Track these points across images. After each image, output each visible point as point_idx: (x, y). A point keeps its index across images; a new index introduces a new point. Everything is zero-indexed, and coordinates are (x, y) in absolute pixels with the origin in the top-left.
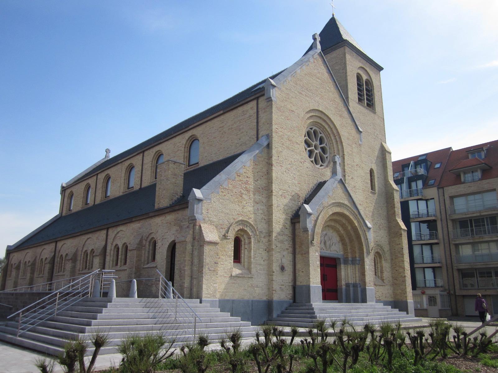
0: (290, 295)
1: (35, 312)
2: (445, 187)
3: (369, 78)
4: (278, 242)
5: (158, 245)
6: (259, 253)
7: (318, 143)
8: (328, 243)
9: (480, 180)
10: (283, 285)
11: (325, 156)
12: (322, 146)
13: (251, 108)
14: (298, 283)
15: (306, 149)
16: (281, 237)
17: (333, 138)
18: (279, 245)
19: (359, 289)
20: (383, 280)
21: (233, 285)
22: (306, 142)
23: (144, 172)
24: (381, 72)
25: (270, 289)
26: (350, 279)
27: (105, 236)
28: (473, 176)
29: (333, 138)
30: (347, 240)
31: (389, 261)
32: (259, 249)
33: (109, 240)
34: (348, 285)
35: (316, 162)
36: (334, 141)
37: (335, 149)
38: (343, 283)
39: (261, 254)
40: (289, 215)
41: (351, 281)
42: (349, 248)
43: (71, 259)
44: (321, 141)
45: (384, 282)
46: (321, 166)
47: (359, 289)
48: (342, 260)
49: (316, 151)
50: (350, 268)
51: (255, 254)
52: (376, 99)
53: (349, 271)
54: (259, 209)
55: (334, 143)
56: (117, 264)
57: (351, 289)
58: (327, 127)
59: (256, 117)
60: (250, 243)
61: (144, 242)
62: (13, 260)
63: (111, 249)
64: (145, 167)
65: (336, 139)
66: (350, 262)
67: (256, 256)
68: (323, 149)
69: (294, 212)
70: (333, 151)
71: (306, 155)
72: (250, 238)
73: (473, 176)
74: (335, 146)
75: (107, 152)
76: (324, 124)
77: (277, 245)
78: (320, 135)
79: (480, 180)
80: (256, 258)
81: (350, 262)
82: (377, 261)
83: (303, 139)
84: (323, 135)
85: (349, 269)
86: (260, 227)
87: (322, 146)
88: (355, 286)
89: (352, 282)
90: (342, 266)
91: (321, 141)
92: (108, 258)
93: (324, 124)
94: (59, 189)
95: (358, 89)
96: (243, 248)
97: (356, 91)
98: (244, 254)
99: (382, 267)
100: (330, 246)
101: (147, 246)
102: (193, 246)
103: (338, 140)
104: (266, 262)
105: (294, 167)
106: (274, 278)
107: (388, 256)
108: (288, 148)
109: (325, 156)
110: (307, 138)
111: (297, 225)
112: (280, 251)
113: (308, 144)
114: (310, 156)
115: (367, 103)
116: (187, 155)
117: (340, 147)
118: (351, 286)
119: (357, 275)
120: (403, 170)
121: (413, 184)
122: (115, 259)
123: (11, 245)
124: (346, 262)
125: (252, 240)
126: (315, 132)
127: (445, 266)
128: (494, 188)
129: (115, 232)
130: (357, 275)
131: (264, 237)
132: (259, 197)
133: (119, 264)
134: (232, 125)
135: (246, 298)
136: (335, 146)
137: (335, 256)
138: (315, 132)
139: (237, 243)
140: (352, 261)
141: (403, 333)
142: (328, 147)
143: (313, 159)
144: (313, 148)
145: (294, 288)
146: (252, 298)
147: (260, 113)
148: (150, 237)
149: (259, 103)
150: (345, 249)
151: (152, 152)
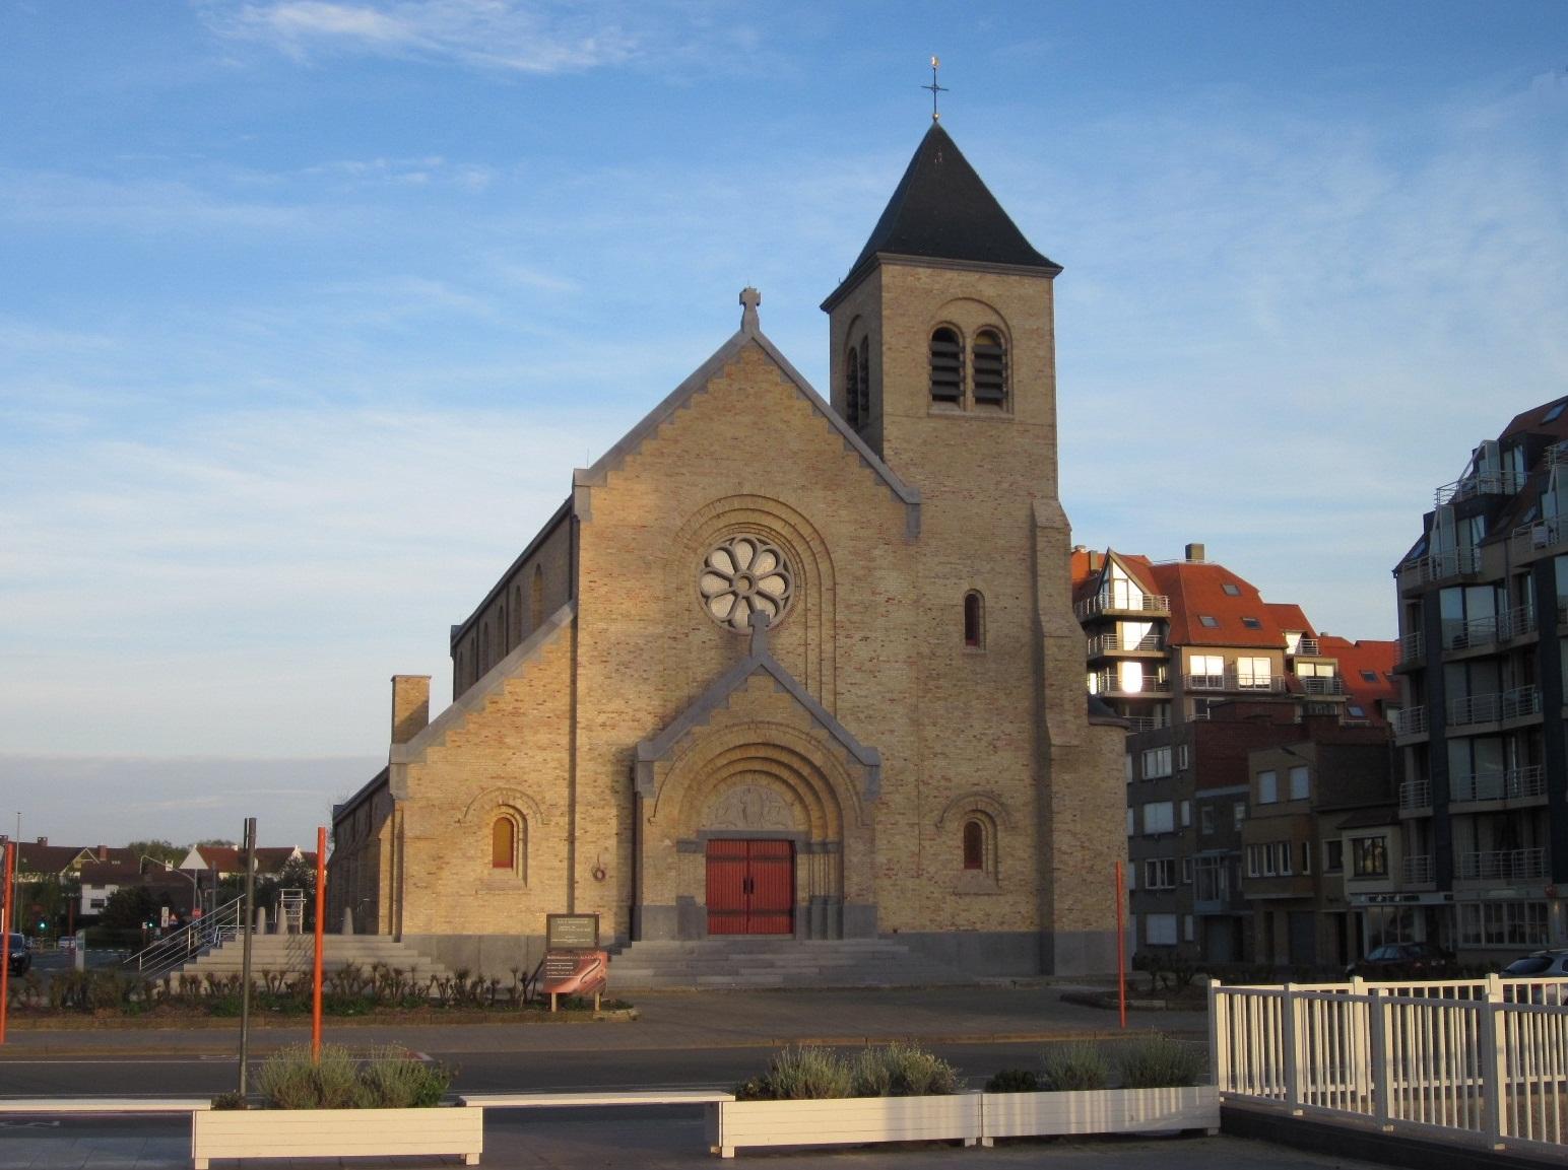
0: (624, 925)
3: (993, 319)
4: (591, 821)
6: (548, 847)
10: (604, 907)
16: (601, 810)
20: (998, 880)
21: (483, 909)
24: (1057, 280)
26: (817, 888)
32: (547, 840)
39: (554, 847)
40: (625, 763)
41: (820, 891)
45: (997, 884)
50: (819, 862)
51: (537, 850)
54: (549, 760)
58: (777, 525)
67: (540, 852)
70: (803, 579)
75: (745, 304)
77: (588, 829)
80: (539, 858)
82: (987, 832)
86: (550, 796)
89: (822, 894)
112: (594, 839)
117: (824, 566)
119: (832, 877)
123: (1423, 533)
124: (809, 848)
130: (832, 877)
132: (550, 736)
135: (512, 932)
141: (95, 904)
142: (792, 572)
146: (528, 932)
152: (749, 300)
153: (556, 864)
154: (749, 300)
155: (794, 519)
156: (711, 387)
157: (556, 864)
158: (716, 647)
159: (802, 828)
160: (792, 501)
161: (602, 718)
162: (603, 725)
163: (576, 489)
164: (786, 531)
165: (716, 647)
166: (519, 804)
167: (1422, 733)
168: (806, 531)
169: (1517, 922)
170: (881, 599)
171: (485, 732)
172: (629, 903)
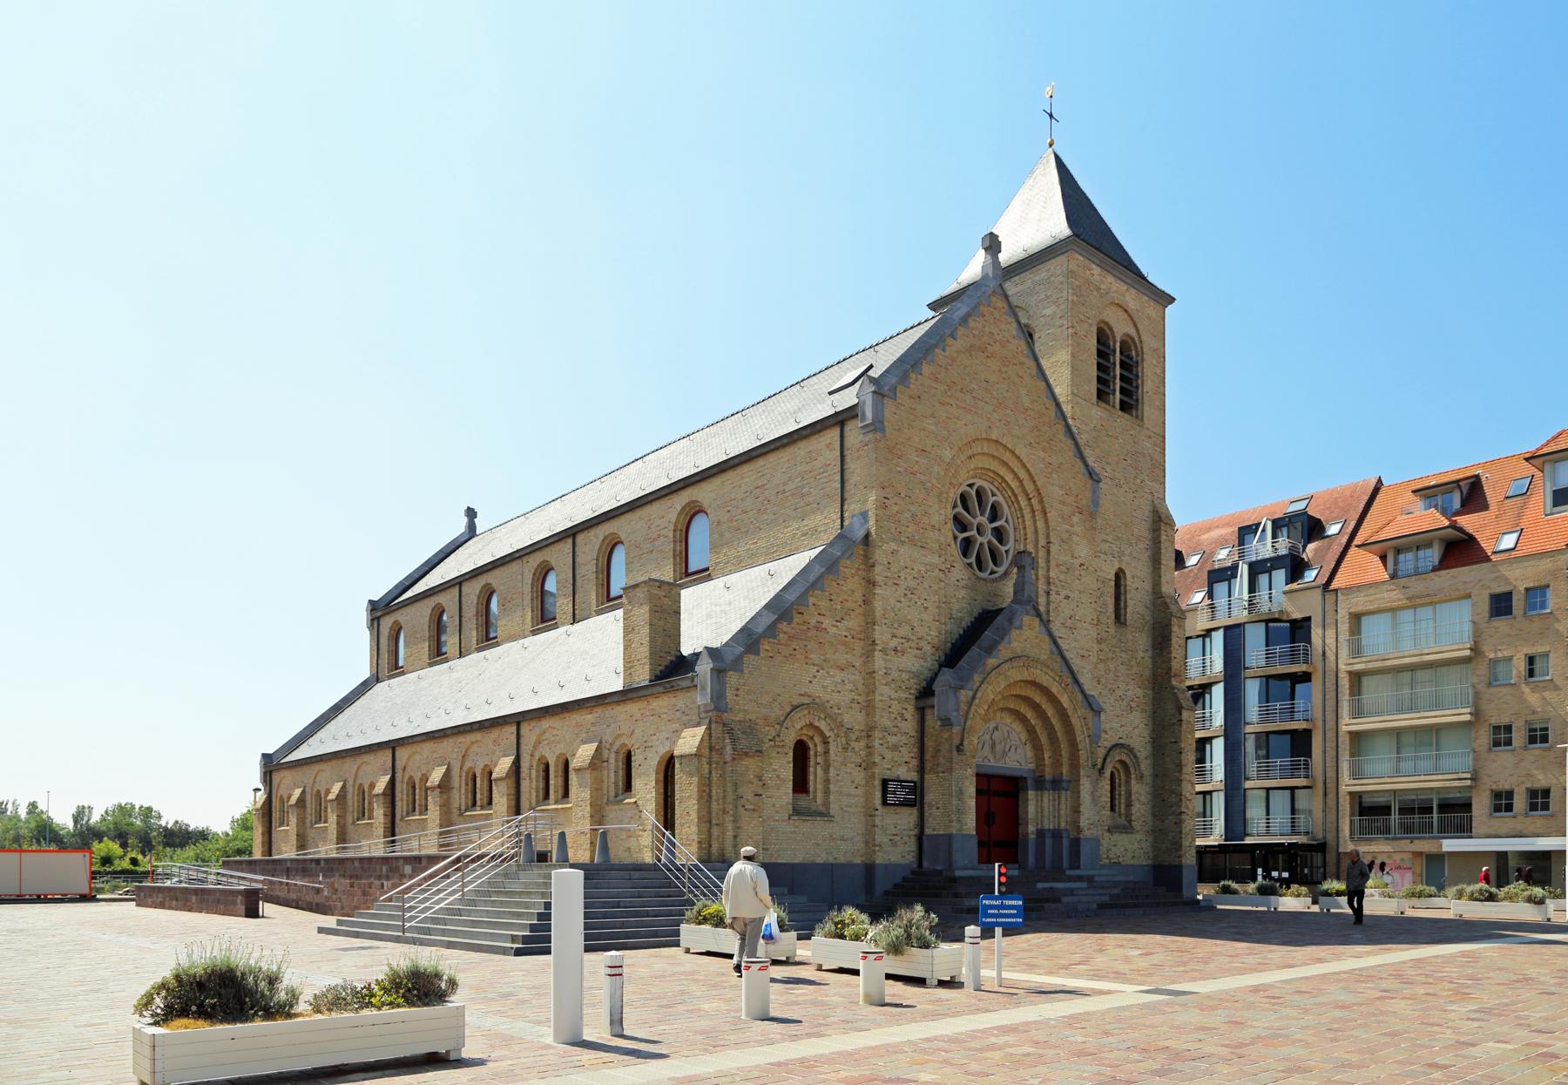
1: (424, 891)
3: (1133, 332)
5: (637, 759)
7: (984, 520)
8: (998, 748)
9: (1435, 569)
11: (1003, 549)
13: (828, 445)
15: (955, 538)
17: (1023, 503)
18: (888, 755)
19: (1065, 842)
22: (956, 518)
23: (579, 583)
24: (1169, 310)
25: (870, 842)
27: (513, 739)
28: (1417, 559)
29: (1023, 503)
30: (1044, 739)
31: (1148, 779)
33: (523, 747)
34: (1041, 833)
36: (1026, 511)
37: (1030, 531)
38: (1031, 828)
42: (1047, 755)
43: (439, 786)
44: (994, 516)
47: (1065, 842)
48: (1030, 782)
49: (980, 539)
52: (1148, 386)
53: (1045, 805)
55: (1028, 516)
56: (547, 796)
57: (1048, 842)
58: (1009, 478)
59: (838, 468)
60: (827, 752)
61: (605, 754)
62: (283, 786)
63: (531, 766)
64: (580, 571)
66: (1048, 785)
68: (999, 534)
69: (924, 684)
71: (955, 550)
72: (826, 742)
73: (1417, 559)
74: (1029, 523)
76: (1002, 471)
79: (1435, 569)
81: (1048, 785)
83: (950, 513)
84: (1000, 498)
85: (1046, 800)
88: (1057, 834)
90: (1031, 794)
91: (994, 516)
92: (525, 784)
93: (1002, 471)
94: (362, 617)
95: (1100, 367)
96: (812, 763)
97: (1094, 372)
98: (816, 775)
99: (1129, 794)
100: (1005, 753)
101: (612, 761)
102: (710, 763)
103: (1037, 507)
104: (861, 791)
105: (926, 585)
106: (878, 821)
107: (1146, 767)
108: (912, 541)
109: (1003, 549)
110: (960, 509)
111: (928, 712)
113: (961, 525)
114: (965, 553)
115: (1122, 401)
116: (680, 547)
117: (1040, 525)
118: (1048, 835)
120: (1241, 542)
121: (1263, 579)
122: (541, 785)
124: (1040, 784)
125: (832, 747)
126: (980, 494)
127: (1320, 785)
129: (537, 731)
131: (857, 740)
133: (552, 796)
134: (785, 484)
135: (819, 860)
136: (1029, 523)
137: (1018, 774)
138: (980, 494)
139: (801, 753)
143: (973, 560)
144: (974, 532)
145: (920, 838)
147: (848, 459)
148: (618, 743)
149: (846, 434)
150: (1039, 757)
151: (596, 536)
152: (471, 513)
153: (853, 790)
154: (471, 513)
155: (1022, 474)
156: (971, 323)
157: (853, 790)
158: (965, 587)
159: (1032, 766)
160: (1022, 452)
161: (894, 643)
162: (895, 650)
163: (276, 778)
164: (1014, 484)
165: (965, 587)
166: (823, 725)
167: (1302, 899)
168: (1030, 487)
169: (1395, 817)
170: (1077, 562)
171: (794, 645)
172: (916, 832)
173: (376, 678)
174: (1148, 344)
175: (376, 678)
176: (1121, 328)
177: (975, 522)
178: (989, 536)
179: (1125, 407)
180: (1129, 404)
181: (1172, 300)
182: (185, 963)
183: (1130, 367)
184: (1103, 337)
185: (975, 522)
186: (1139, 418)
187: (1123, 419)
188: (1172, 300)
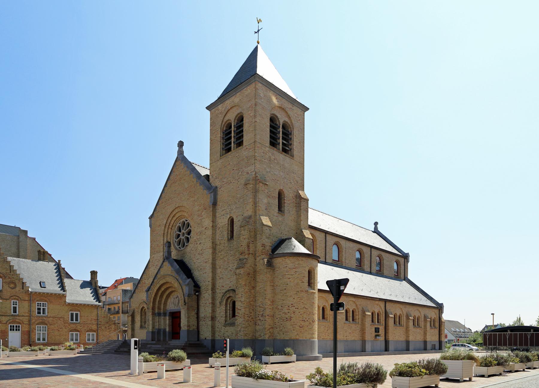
2: (198, 174)
3: (287, 120)
7: (181, 237)
11: (180, 225)
12: (179, 233)
14: (332, 359)
24: (306, 113)
35: (188, 225)
44: (179, 235)
46: (186, 220)
49: (185, 232)
65: (172, 219)
71: (192, 234)
78: (177, 240)
87: (179, 233)
109: (180, 225)
110: (186, 244)
113: (188, 240)
128: (443, 348)
139: (232, 237)
140: (163, 313)
143: (189, 228)
144: (185, 235)
173: (181, 153)
174: (296, 124)
175: (181, 153)
176: (282, 119)
177: (184, 238)
178: (183, 231)
179: (285, 151)
180: (287, 150)
181: (307, 109)
182: (369, 362)
183: (287, 136)
184: (273, 120)
185: (184, 238)
186: (292, 156)
187: (281, 157)
188: (307, 109)
